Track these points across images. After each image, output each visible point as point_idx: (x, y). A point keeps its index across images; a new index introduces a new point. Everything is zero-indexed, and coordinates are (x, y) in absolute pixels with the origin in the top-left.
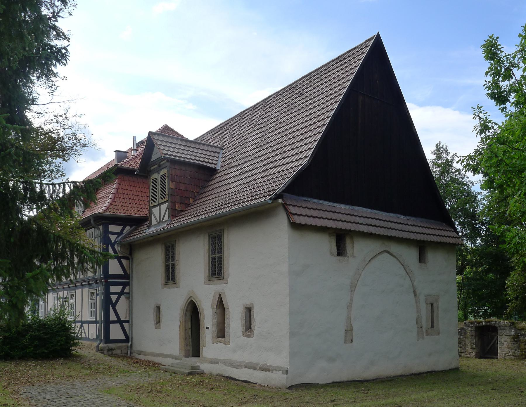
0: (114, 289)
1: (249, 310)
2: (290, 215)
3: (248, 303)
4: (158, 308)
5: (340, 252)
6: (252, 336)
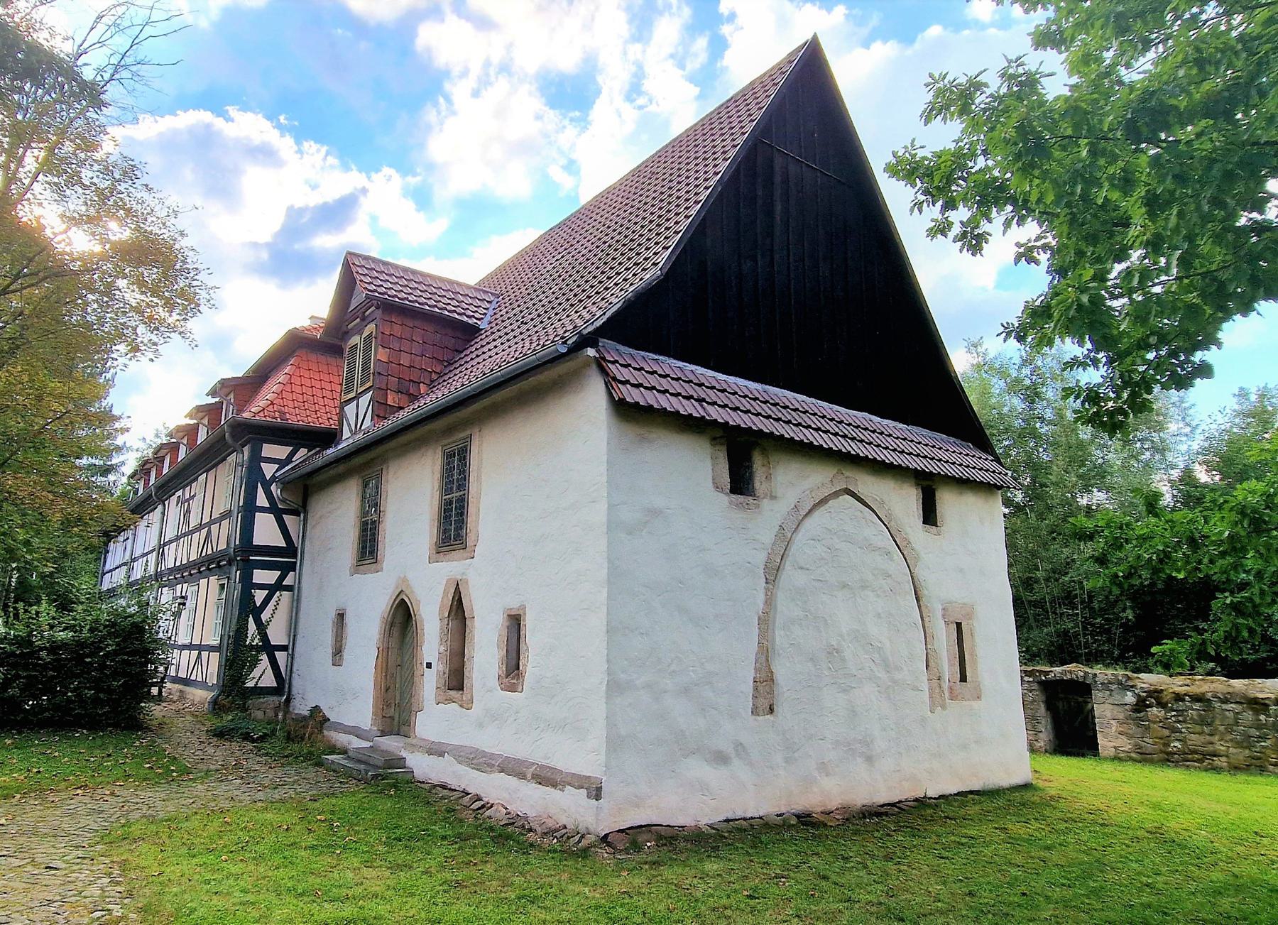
0: (261, 576)
1: (515, 623)
2: (613, 383)
3: (513, 604)
4: (341, 616)
5: (740, 483)
6: (520, 690)
